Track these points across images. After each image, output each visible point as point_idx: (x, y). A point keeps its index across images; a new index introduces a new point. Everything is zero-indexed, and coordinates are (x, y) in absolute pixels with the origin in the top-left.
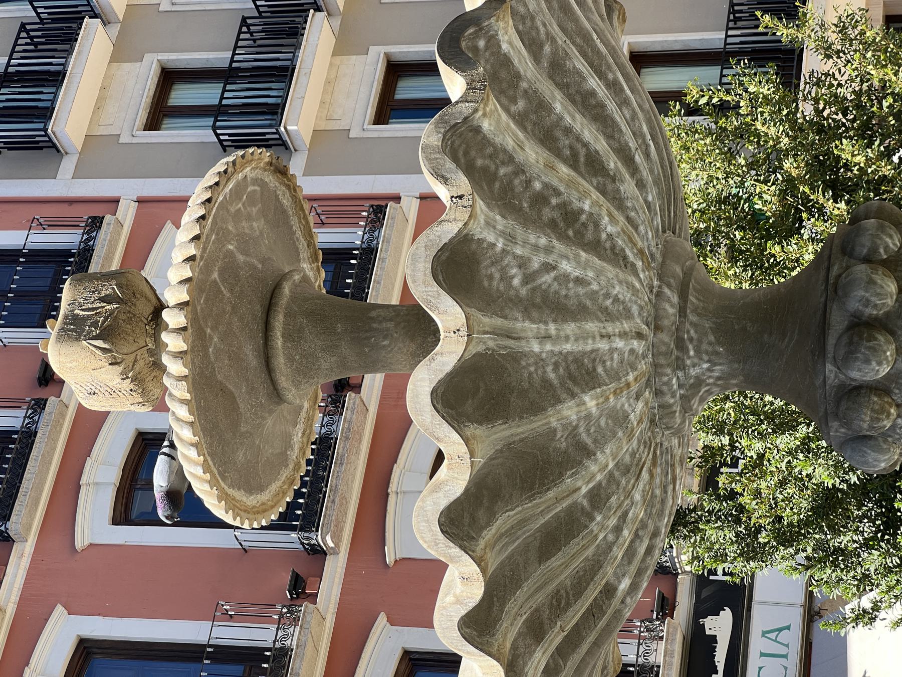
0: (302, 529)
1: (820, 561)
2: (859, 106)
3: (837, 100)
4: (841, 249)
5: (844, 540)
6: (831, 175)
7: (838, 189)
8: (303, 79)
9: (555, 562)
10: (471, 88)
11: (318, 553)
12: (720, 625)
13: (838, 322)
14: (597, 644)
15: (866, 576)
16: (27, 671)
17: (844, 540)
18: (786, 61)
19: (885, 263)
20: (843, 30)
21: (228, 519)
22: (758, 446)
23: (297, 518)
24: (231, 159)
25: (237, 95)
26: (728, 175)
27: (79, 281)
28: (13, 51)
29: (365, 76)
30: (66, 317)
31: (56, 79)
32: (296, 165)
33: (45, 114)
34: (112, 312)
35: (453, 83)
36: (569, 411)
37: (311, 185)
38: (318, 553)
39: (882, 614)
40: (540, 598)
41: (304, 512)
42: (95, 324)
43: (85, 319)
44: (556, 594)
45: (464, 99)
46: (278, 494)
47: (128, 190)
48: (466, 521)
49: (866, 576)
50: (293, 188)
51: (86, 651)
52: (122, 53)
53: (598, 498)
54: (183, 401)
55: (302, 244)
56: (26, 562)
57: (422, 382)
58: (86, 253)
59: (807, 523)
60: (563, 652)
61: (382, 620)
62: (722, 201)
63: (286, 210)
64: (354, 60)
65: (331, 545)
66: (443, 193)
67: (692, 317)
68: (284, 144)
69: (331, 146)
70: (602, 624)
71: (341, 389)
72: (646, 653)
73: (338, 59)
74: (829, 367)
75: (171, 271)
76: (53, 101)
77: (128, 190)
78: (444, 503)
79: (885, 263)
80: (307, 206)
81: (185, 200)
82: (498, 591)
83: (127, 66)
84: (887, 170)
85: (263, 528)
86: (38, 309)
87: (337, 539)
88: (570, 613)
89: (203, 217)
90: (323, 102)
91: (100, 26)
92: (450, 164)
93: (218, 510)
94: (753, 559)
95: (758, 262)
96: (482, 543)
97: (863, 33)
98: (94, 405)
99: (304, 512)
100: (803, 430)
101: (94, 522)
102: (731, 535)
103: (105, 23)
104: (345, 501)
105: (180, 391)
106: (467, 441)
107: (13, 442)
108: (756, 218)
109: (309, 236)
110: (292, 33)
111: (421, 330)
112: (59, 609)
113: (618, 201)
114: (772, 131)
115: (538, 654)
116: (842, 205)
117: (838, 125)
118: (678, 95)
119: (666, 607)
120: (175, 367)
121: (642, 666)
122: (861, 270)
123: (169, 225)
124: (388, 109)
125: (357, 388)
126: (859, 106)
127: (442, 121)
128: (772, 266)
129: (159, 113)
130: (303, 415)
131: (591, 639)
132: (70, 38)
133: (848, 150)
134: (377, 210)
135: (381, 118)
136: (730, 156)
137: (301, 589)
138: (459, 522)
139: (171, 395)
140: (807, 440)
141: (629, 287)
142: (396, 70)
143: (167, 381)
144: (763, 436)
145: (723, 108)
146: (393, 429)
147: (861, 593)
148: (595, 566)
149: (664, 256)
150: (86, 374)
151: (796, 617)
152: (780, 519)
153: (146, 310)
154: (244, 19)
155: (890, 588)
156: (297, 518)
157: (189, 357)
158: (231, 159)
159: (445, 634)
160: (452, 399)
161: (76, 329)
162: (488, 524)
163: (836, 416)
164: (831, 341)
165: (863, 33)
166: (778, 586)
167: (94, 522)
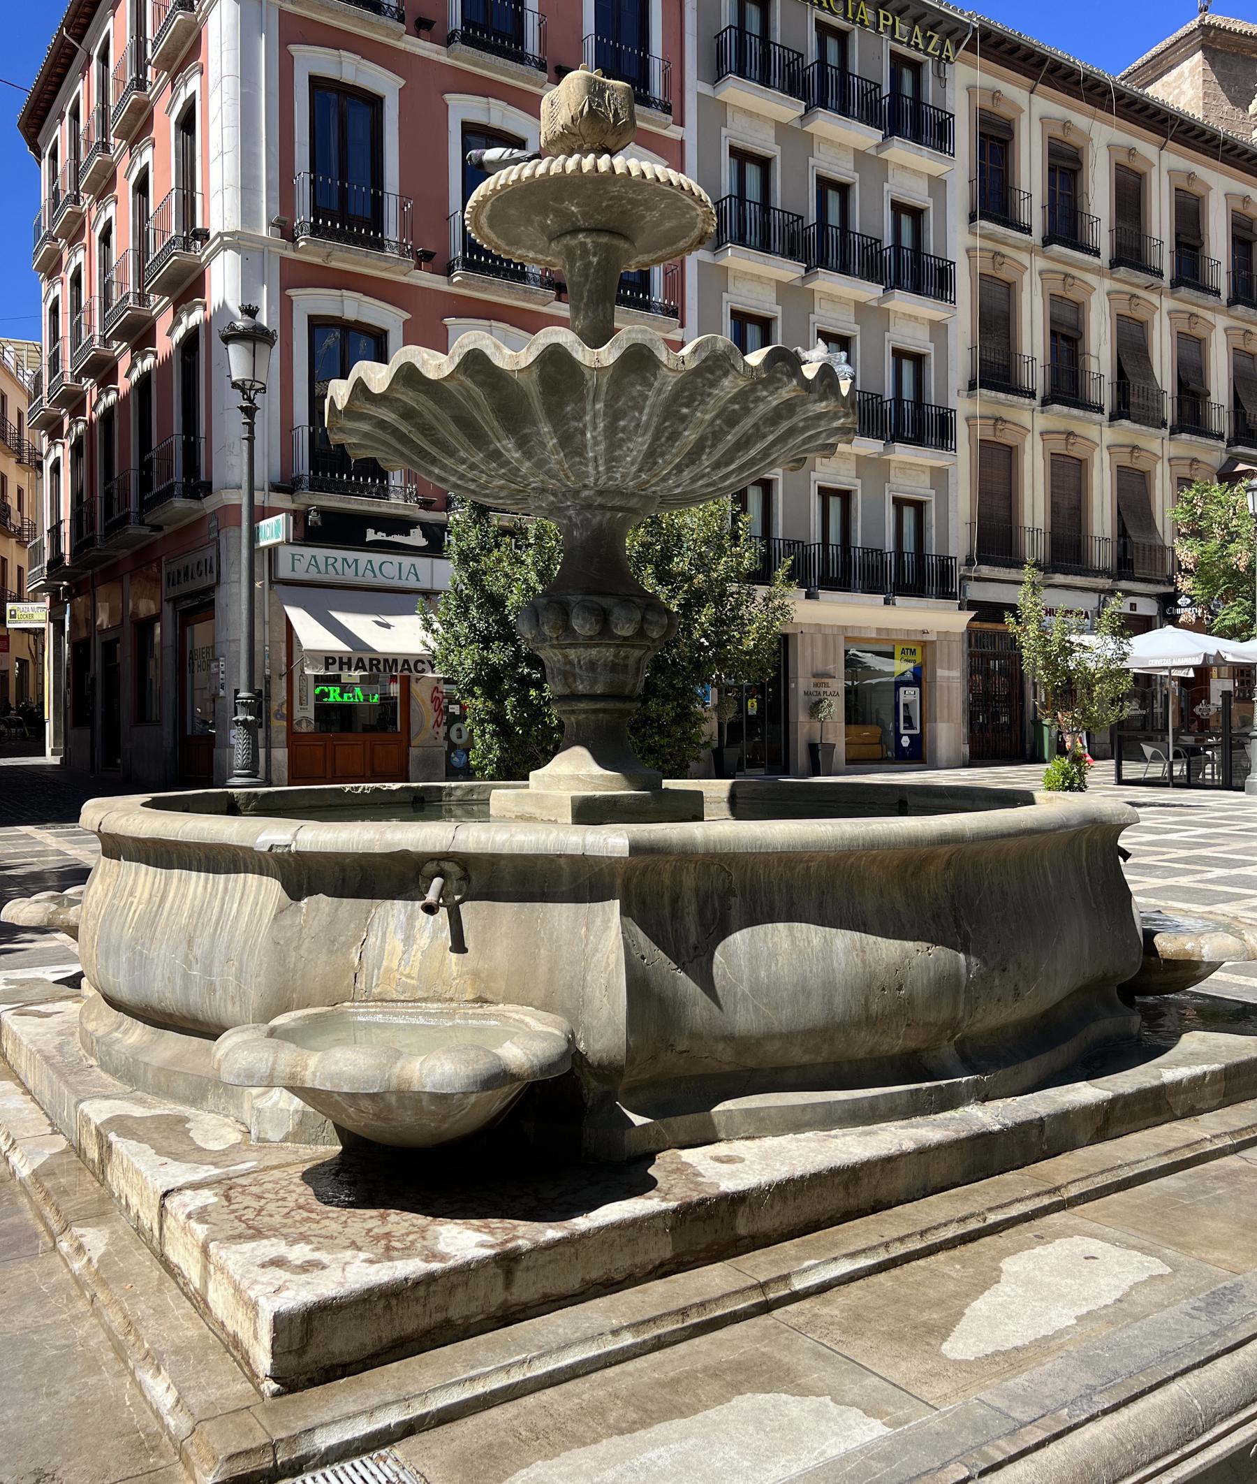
0: (464, 259)
1: (461, 598)
2: (734, 618)
3: (738, 606)
4: (651, 603)
5: (474, 612)
6: (695, 601)
7: (686, 607)
8: (761, 259)
9: (453, 427)
10: (753, 369)
11: (448, 271)
12: (416, 538)
13: (606, 602)
14: (402, 455)
15: (452, 625)
16: (358, 58)
17: (474, 612)
18: (762, 575)
19: (642, 628)
20: (780, 608)
21: (470, 203)
22: (529, 561)
23: (472, 256)
24: (710, 204)
25: (752, 212)
26: (695, 541)
27: (628, 94)
28: (784, 48)
29: (763, 302)
30: (604, 83)
31: (765, 81)
32: (702, 255)
33: (741, 73)
34: (608, 118)
35: (755, 358)
36: (546, 428)
37: (691, 262)
38: (448, 271)
39: (430, 635)
40: (429, 417)
41: (478, 259)
42: (599, 105)
43: (603, 98)
44: (432, 428)
45: (746, 364)
46: (488, 238)
47: (689, 133)
48: (477, 367)
49: (452, 625)
50: (690, 249)
51: (375, 102)
52: (782, 130)
53: (496, 455)
54: (548, 169)
55: (654, 256)
56: (434, 56)
57: (565, 337)
58: (646, 101)
59: (483, 590)
60: (396, 432)
61: (407, 316)
62: (679, 536)
63: (673, 249)
64: (773, 296)
65: (455, 280)
66: (686, 351)
67: (608, 515)
68: (719, 246)
69: (716, 279)
70: (415, 458)
71: (559, 288)
72: (396, 492)
73: (774, 284)
74: (580, 597)
75: (633, 162)
76: (750, 78)
77: (689, 133)
78: (488, 352)
79: (642, 628)
80: (678, 258)
81: (682, 171)
82: (432, 388)
83: (772, 133)
84: (696, 635)
85: (464, 227)
86: (609, 63)
87: (458, 284)
88: (421, 437)
89: (671, 184)
90: (746, 273)
91: (799, 114)
92: (704, 355)
93: (475, 196)
94: (460, 559)
95: (642, 559)
96: (463, 378)
97: (778, 619)
98: (544, 105)
99: (478, 259)
100: (540, 588)
101: (464, 108)
102: (473, 545)
103: (801, 117)
104: (484, 290)
105: (555, 168)
106: (528, 367)
107: (517, 47)
108: (669, 559)
109: (657, 261)
110: (791, 252)
111: (598, 336)
112: (403, 82)
113: (679, 469)
114: (721, 567)
115: (394, 416)
116: (675, 609)
117: (724, 607)
118: (744, 510)
119: (426, 505)
120: (571, 164)
121: (387, 489)
122: (637, 615)
123: (667, 163)
124: (741, 319)
125: (559, 299)
126: (734, 618)
127: (732, 350)
128: (639, 568)
129: (741, 156)
130: (540, 257)
131: (404, 450)
132: (792, 92)
133: (708, 611)
134: (675, 312)
135: (735, 314)
136: (706, 542)
137: (424, 259)
138: (475, 362)
139: (552, 161)
140: (534, 590)
141: (627, 473)
142: (765, 325)
143: (562, 157)
144: (535, 563)
145: (735, 538)
146: (530, 323)
147: (442, 623)
148: (451, 453)
149: (646, 497)
150: (564, 99)
151: (425, 584)
152: (485, 574)
153: (610, 142)
154: (802, 218)
155: (446, 640)
156: (472, 256)
157: (578, 174)
158: (710, 204)
159: (402, 354)
160: (555, 358)
161: (595, 91)
162: (475, 382)
163: (550, 602)
164: (595, 598)
165: (778, 619)
166: (444, 573)
167: (464, 108)
